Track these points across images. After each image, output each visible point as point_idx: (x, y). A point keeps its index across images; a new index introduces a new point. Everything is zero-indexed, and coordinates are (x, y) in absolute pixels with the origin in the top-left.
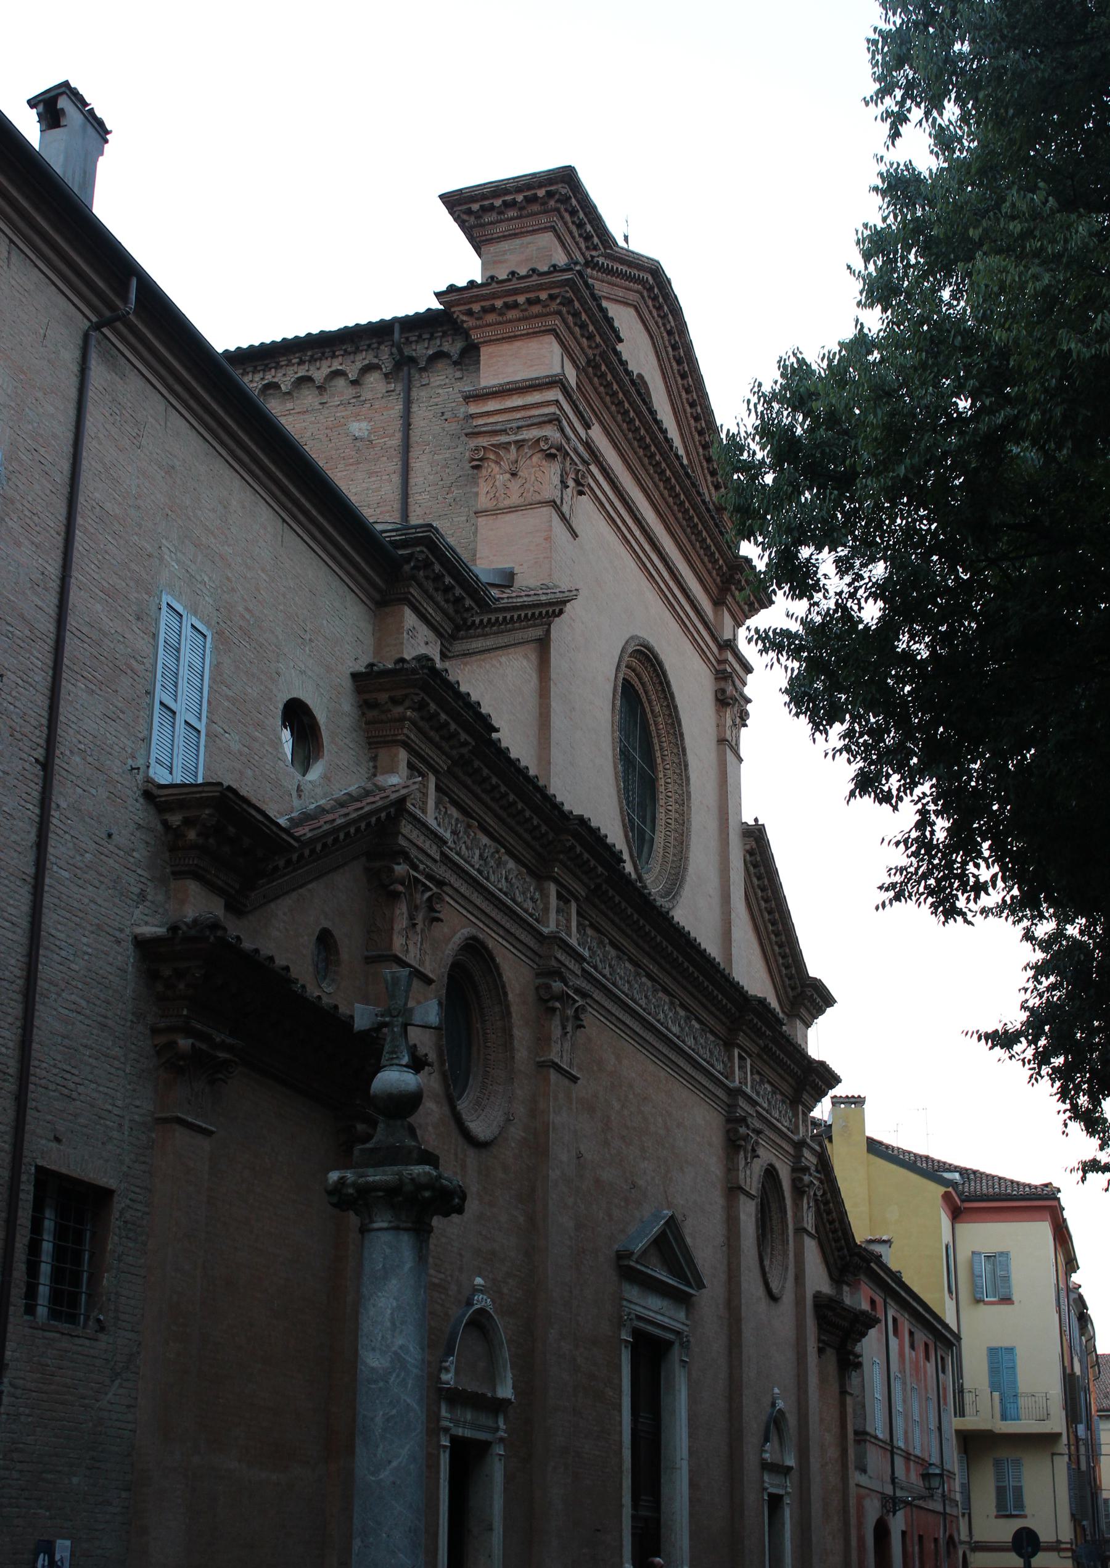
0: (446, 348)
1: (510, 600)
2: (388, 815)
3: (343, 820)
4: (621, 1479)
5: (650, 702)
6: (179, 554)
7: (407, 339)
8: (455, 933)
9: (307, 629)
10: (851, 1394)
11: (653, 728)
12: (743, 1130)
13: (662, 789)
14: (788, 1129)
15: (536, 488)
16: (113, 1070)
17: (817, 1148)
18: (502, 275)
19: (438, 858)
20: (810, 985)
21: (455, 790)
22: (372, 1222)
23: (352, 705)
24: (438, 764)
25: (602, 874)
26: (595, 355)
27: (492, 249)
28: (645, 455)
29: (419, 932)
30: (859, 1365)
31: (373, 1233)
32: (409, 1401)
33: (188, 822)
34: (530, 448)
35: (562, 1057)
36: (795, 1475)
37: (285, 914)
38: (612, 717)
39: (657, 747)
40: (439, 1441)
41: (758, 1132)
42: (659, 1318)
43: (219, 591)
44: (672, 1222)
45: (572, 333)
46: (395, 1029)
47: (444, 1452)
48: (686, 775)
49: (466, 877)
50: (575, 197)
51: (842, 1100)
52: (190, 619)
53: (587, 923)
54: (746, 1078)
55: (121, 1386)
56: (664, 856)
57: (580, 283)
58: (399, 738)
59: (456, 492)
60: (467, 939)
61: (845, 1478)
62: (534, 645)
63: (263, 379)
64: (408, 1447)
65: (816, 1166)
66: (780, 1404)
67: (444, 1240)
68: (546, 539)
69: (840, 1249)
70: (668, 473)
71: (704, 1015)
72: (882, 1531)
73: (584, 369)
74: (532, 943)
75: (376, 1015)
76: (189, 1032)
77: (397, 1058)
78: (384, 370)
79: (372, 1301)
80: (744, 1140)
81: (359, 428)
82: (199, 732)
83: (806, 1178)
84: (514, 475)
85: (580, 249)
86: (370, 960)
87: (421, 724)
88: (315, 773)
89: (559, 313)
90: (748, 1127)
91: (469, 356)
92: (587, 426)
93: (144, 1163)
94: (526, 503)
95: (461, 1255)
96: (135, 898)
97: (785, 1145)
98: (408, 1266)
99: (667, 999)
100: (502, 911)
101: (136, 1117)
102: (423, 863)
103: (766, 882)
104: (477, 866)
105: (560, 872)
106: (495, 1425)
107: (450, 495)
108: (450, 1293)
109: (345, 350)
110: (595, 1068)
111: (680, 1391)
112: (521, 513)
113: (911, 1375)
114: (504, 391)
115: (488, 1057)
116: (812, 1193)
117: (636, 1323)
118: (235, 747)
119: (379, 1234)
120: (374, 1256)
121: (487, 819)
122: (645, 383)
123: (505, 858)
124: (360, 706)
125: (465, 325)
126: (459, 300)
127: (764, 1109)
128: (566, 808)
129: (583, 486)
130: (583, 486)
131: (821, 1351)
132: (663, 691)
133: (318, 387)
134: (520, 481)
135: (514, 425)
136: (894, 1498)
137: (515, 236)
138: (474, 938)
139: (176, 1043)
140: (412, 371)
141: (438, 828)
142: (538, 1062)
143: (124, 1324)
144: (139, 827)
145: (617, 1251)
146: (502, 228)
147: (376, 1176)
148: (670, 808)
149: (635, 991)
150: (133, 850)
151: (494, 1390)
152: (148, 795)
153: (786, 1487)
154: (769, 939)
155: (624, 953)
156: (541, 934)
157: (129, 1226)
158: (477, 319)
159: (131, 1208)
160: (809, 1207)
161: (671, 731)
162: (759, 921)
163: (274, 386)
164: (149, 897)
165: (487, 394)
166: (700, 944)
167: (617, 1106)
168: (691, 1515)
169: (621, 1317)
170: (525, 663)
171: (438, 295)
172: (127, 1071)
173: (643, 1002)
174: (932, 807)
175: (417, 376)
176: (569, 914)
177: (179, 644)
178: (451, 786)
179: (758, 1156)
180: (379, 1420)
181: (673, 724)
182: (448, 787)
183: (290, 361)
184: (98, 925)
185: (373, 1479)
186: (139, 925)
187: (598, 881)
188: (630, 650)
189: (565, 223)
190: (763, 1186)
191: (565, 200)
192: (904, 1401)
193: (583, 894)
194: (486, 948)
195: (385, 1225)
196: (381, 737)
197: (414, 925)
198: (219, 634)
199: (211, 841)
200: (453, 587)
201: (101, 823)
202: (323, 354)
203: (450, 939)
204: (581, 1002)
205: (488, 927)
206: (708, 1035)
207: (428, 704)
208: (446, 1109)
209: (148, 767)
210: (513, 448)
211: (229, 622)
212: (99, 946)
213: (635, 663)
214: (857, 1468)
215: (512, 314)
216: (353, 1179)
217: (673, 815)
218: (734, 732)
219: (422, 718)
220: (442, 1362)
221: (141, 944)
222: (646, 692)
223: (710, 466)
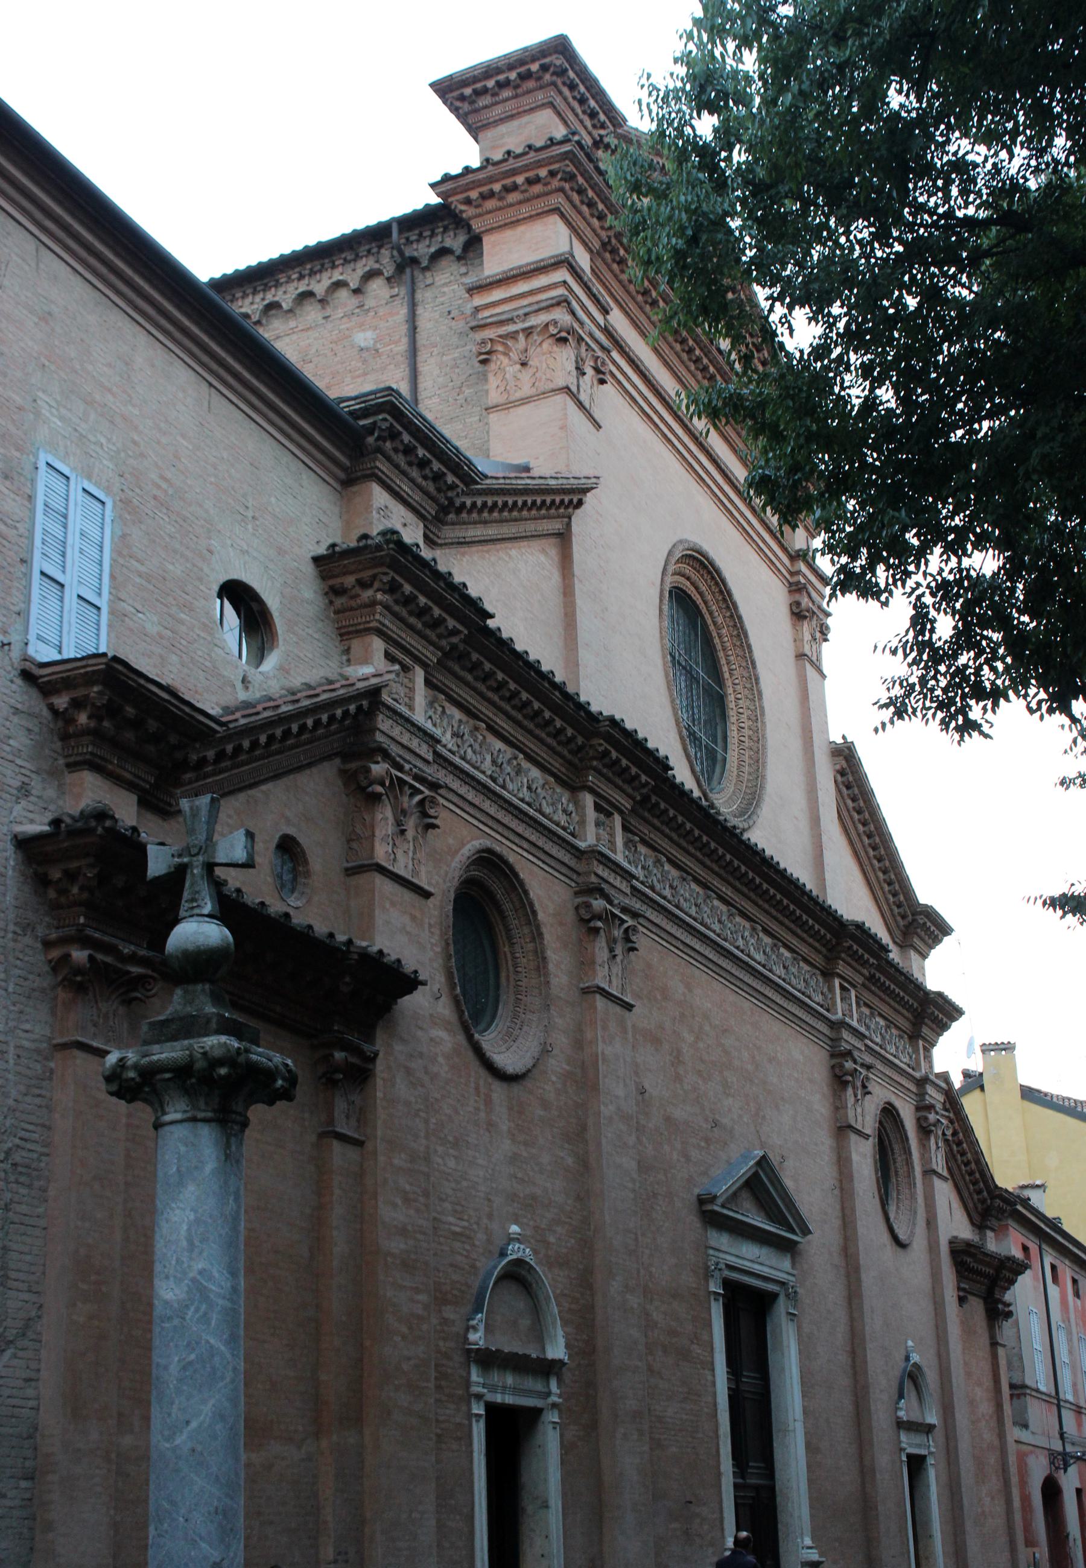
0: (448, 243)
1: (508, 481)
2: (359, 708)
3: (290, 707)
4: (718, 1444)
5: (711, 613)
6: (62, 410)
7: (407, 239)
8: (463, 845)
9: (250, 505)
10: (1004, 1346)
11: (717, 641)
12: (849, 1065)
13: (732, 705)
14: (909, 1066)
15: (548, 376)
17: (943, 1085)
18: (497, 156)
19: (430, 758)
20: (921, 913)
21: (454, 687)
22: (164, 1113)
23: (315, 592)
24: (426, 657)
25: (647, 783)
26: (609, 237)
27: (489, 134)
28: (683, 350)
29: (411, 839)
30: (1009, 1314)
31: (166, 1128)
32: (212, 1341)
33: (77, 704)
34: (539, 334)
35: (610, 981)
36: (939, 1433)
37: (229, 817)
38: (660, 622)
39: (723, 661)
40: (470, 1409)
41: (869, 1067)
42: (757, 1268)
43: (123, 455)
44: (763, 1162)
45: (580, 213)
46: (195, 871)
47: (477, 1421)
49: (473, 783)
50: (572, 69)
51: (991, 1047)
52: (77, 484)
53: (637, 839)
54: (851, 1011)
55: (15, 1356)
56: (738, 776)
57: (581, 156)
58: (371, 625)
59: (467, 392)
60: (479, 852)
61: (1002, 1435)
62: (553, 540)
63: (263, 299)
64: (212, 1402)
65: (944, 1104)
66: (915, 1358)
67: (465, 1184)
68: (561, 428)
69: (979, 1192)
70: (712, 369)
71: (794, 942)
72: (1051, 1491)
73: (598, 253)
74: (566, 858)
75: (173, 856)
76: (85, 942)
77: (198, 906)
78: (386, 274)
79: (165, 1215)
80: (852, 1075)
81: (364, 338)
82: (98, 609)
83: (932, 1117)
84: (524, 364)
85: (585, 128)
87: (397, 608)
88: (271, 662)
89: (561, 190)
90: (855, 1062)
91: (474, 244)
92: (605, 311)
93: (39, 1096)
95: (489, 1200)
96: (15, 792)
97: (905, 1082)
98: (210, 1167)
99: (748, 925)
100: (523, 822)
101: (26, 1044)
102: (409, 762)
103: (862, 804)
104: (489, 773)
106: (545, 1390)
107: (461, 396)
108: (477, 1243)
110: (659, 997)
111: (789, 1346)
112: (533, 404)
113: (1077, 1324)
114: (508, 278)
115: (519, 983)
116: (940, 1133)
117: (727, 1273)
118: (153, 629)
119: (172, 1128)
120: (167, 1157)
121: (498, 721)
123: (526, 765)
124: (326, 594)
125: (464, 215)
126: (455, 188)
127: (877, 1044)
128: (594, 708)
129: (604, 373)
130: (604, 373)
131: (962, 1300)
132: (724, 600)
133: (321, 301)
134: (532, 371)
135: (521, 312)
136: (1065, 1455)
137: (512, 117)
138: (489, 851)
139: (70, 955)
140: (416, 273)
141: (434, 729)
142: (582, 989)
143: (16, 1283)
144: (17, 711)
145: (699, 1195)
146: (497, 111)
147: (166, 1053)
148: (742, 725)
149: (705, 916)
150: (9, 738)
151: (543, 1350)
152: (27, 676)
153: (929, 1447)
154: (872, 865)
155: (688, 873)
156: (577, 849)
157: (20, 1169)
158: (477, 207)
159: (23, 1149)
160: (938, 1148)
161: (738, 643)
162: (859, 846)
163: (273, 307)
164: (34, 792)
165: (491, 284)
166: (778, 863)
167: (690, 1038)
168: (810, 1481)
169: (709, 1267)
170: (542, 558)
171: (433, 186)
172: (10, 990)
173: (716, 927)
174: (928, 600)
175: (421, 277)
176: (612, 828)
177: (66, 509)
178: (447, 682)
179: (869, 1093)
180: (174, 1369)
181: (739, 635)
182: (444, 684)
183: (289, 277)
185: (167, 1445)
186: (21, 823)
187: (645, 791)
188: (678, 555)
189: (565, 99)
190: (880, 1122)
191: (562, 72)
192: (1070, 1352)
194: (506, 862)
195: (178, 1116)
198: (126, 502)
199: (106, 724)
200: (429, 462)
202: (323, 265)
203: (457, 852)
204: (630, 922)
205: (507, 839)
206: (802, 964)
207: (401, 586)
208: (461, 1038)
209: (27, 644)
210: (521, 337)
211: (137, 490)
213: (688, 570)
214: (1015, 1424)
215: (512, 197)
216: (134, 1059)
217: (746, 732)
218: (814, 647)
219: (396, 602)
220: (468, 1320)
221: (24, 844)
222: (705, 603)
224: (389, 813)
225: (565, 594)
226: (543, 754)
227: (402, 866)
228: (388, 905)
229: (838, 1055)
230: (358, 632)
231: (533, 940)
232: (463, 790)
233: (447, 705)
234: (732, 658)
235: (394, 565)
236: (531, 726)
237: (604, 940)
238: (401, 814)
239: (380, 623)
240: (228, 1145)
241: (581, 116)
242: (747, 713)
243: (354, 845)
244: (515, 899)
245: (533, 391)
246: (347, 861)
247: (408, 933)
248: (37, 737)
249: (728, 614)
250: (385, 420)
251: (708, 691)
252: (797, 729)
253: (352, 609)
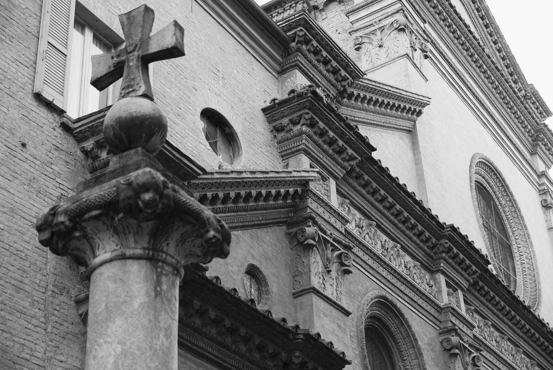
11: (503, 214)
13: (516, 251)
15: (395, 50)
16: (30, 326)
31: (97, 271)
39: (508, 226)
48: (530, 242)
56: (525, 289)
74: (432, 311)
77: (133, 90)
79: (93, 353)
86: (297, 295)
94: (391, 59)
105: (445, 266)
109: (278, 13)
119: (103, 269)
123: (402, 253)
124: (272, 131)
128: (441, 220)
129: (426, 52)
140: (317, 14)
150: (52, 164)
156: (438, 306)
161: (515, 216)
170: (401, 142)
175: (320, 16)
178: (350, 193)
184: (11, 208)
193: (467, 286)
195: (107, 256)
196: (289, 149)
197: (329, 272)
201: (13, 134)
203: (364, 295)
210: (378, 32)
212: (12, 225)
223: (513, 78)
224: (319, 259)
225: (416, 164)
226: (412, 247)
227: (330, 293)
228: (322, 316)
230: (292, 153)
231: (417, 358)
232: (366, 258)
233: (351, 208)
234: (513, 224)
235: (312, 108)
236: (403, 228)
237: (460, 362)
238: (326, 263)
239: (306, 146)
240: (158, 283)
243: (298, 279)
244: (403, 332)
245: (388, 59)
246: (294, 289)
247: (337, 335)
248: (73, 168)
249: (508, 199)
250: (301, 30)
251: (501, 243)
253: (288, 139)
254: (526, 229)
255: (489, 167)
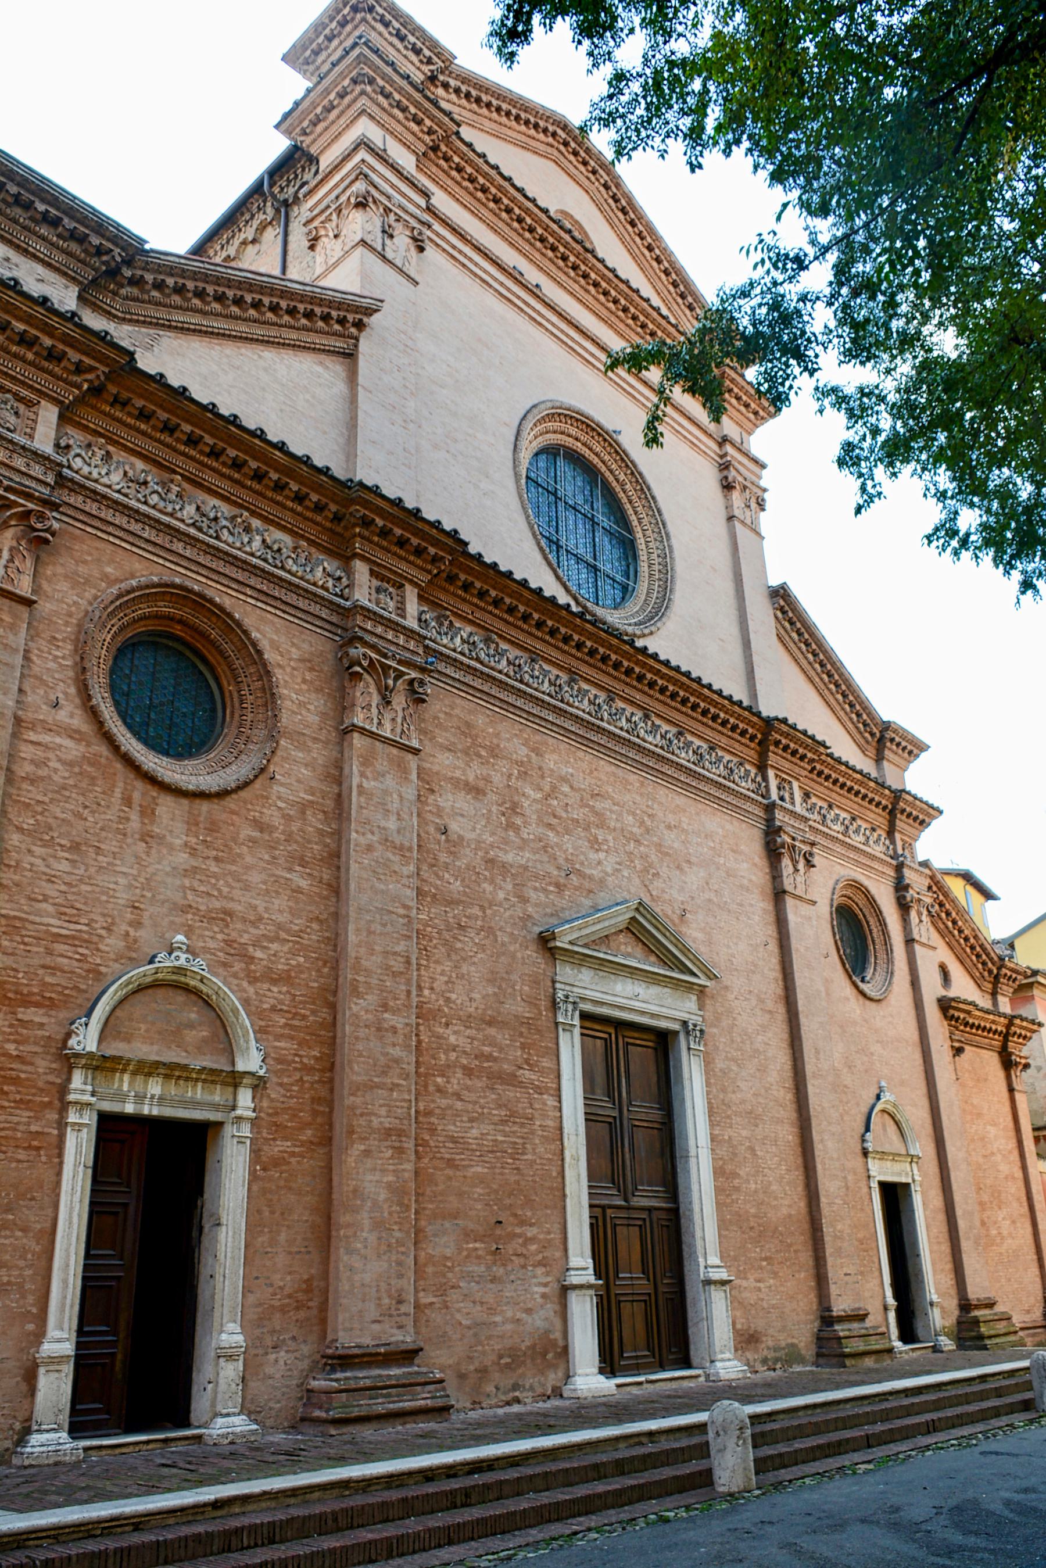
11: (621, 495)
39: (630, 512)
42: (637, 1005)
122: (581, 228)
129: (422, 241)
132: (622, 459)
181: (642, 489)
229: (771, 833)
231: (260, 679)
241: (405, 52)
242: (656, 552)
244: (235, 640)
252: (730, 576)
254: (660, 515)
255: (583, 422)
